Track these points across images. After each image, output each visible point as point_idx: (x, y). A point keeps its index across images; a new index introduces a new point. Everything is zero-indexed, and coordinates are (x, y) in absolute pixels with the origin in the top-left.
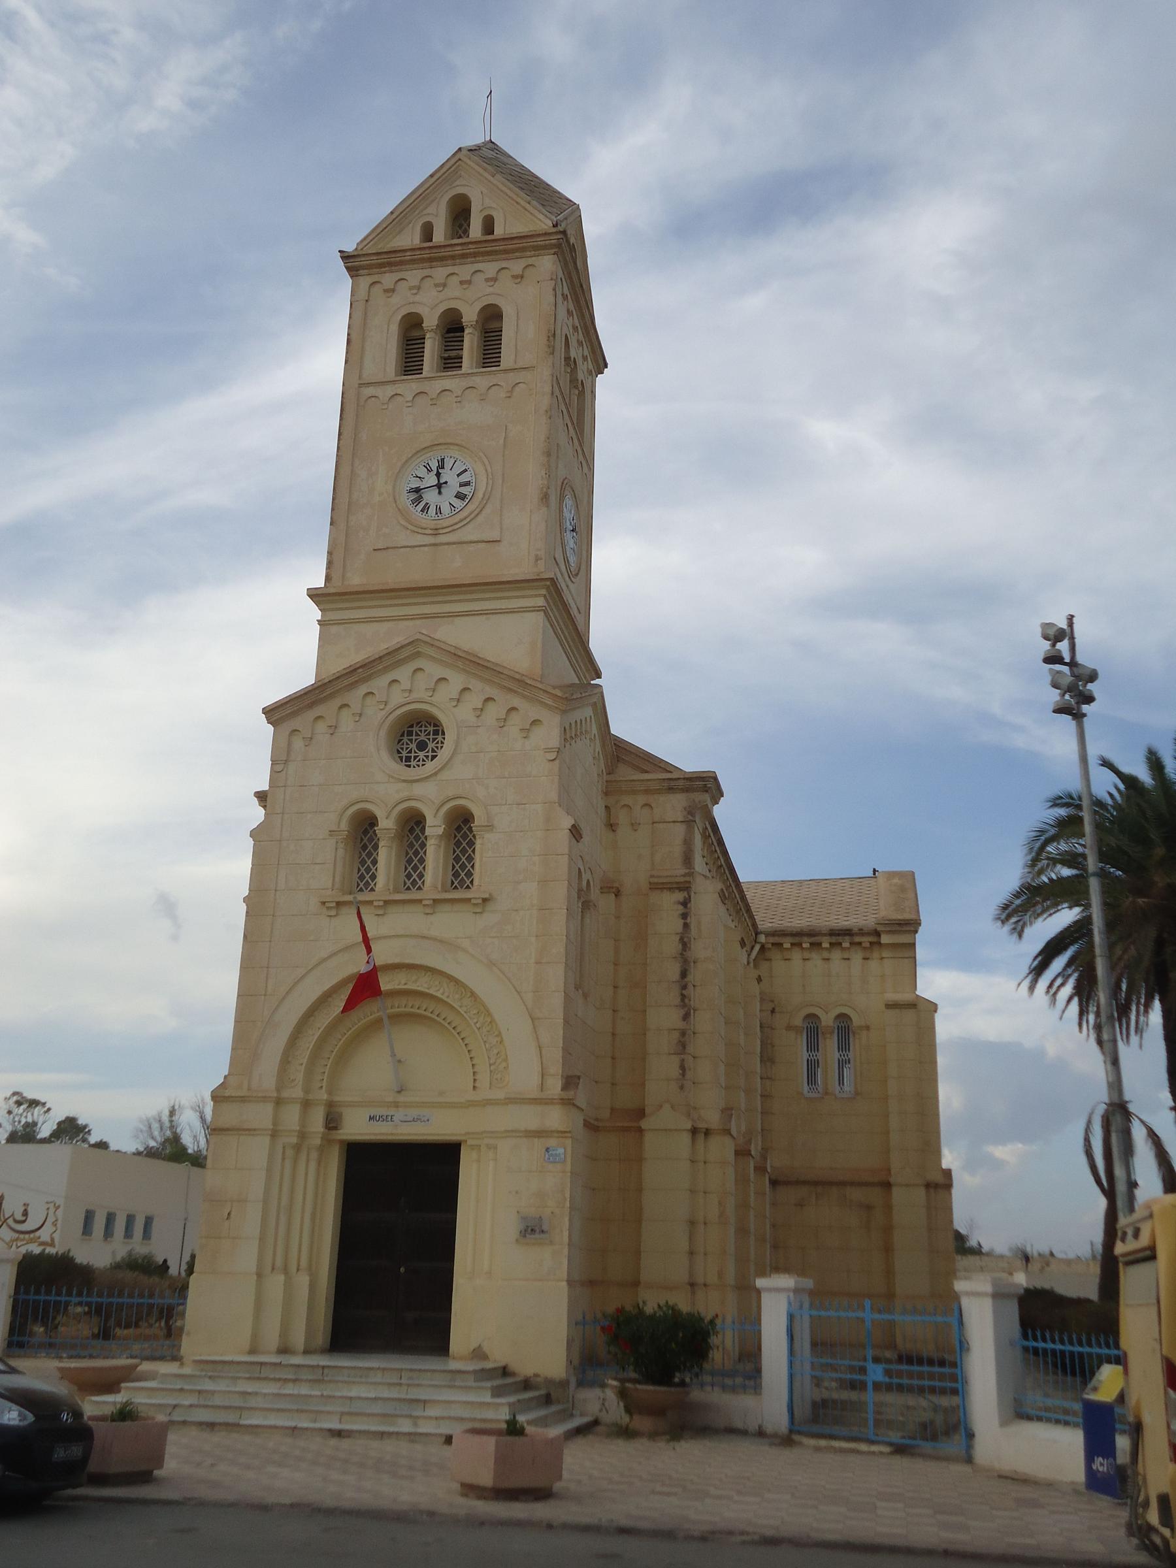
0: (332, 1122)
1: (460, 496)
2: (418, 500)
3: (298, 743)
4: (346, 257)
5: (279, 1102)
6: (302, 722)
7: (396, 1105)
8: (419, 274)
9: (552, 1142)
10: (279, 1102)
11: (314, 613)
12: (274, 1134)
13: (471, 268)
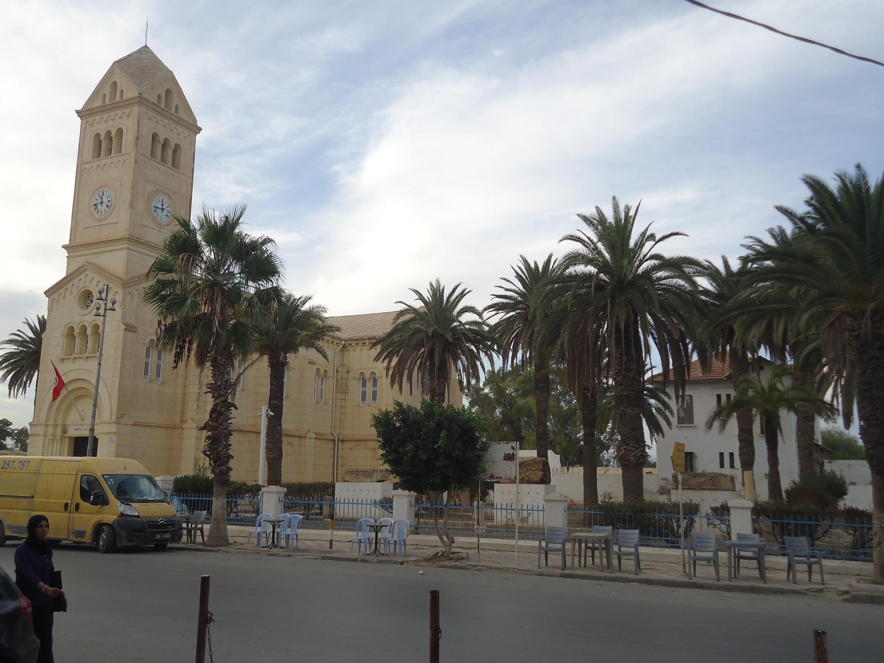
0: (64, 431)
1: (107, 206)
2: (96, 208)
3: (55, 304)
4: (78, 112)
5: (47, 425)
6: (55, 296)
7: (81, 425)
8: (100, 117)
9: (112, 436)
10: (47, 425)
11: (65, 253)
12: (45, 436)
13: (114, 113)
